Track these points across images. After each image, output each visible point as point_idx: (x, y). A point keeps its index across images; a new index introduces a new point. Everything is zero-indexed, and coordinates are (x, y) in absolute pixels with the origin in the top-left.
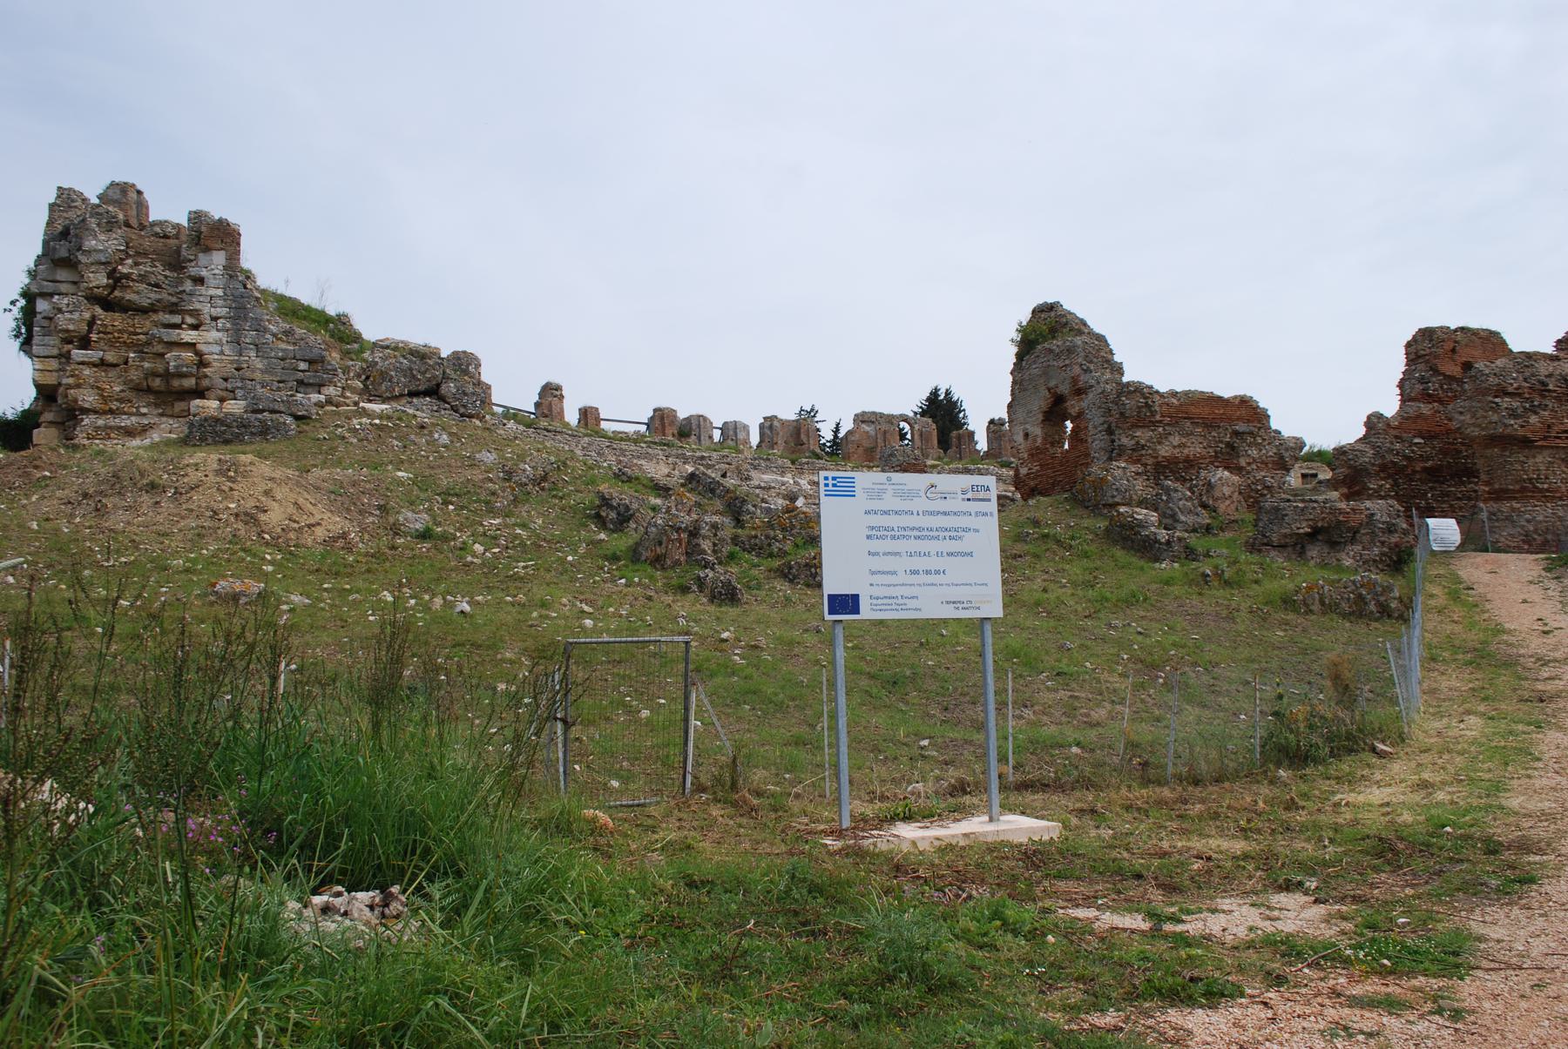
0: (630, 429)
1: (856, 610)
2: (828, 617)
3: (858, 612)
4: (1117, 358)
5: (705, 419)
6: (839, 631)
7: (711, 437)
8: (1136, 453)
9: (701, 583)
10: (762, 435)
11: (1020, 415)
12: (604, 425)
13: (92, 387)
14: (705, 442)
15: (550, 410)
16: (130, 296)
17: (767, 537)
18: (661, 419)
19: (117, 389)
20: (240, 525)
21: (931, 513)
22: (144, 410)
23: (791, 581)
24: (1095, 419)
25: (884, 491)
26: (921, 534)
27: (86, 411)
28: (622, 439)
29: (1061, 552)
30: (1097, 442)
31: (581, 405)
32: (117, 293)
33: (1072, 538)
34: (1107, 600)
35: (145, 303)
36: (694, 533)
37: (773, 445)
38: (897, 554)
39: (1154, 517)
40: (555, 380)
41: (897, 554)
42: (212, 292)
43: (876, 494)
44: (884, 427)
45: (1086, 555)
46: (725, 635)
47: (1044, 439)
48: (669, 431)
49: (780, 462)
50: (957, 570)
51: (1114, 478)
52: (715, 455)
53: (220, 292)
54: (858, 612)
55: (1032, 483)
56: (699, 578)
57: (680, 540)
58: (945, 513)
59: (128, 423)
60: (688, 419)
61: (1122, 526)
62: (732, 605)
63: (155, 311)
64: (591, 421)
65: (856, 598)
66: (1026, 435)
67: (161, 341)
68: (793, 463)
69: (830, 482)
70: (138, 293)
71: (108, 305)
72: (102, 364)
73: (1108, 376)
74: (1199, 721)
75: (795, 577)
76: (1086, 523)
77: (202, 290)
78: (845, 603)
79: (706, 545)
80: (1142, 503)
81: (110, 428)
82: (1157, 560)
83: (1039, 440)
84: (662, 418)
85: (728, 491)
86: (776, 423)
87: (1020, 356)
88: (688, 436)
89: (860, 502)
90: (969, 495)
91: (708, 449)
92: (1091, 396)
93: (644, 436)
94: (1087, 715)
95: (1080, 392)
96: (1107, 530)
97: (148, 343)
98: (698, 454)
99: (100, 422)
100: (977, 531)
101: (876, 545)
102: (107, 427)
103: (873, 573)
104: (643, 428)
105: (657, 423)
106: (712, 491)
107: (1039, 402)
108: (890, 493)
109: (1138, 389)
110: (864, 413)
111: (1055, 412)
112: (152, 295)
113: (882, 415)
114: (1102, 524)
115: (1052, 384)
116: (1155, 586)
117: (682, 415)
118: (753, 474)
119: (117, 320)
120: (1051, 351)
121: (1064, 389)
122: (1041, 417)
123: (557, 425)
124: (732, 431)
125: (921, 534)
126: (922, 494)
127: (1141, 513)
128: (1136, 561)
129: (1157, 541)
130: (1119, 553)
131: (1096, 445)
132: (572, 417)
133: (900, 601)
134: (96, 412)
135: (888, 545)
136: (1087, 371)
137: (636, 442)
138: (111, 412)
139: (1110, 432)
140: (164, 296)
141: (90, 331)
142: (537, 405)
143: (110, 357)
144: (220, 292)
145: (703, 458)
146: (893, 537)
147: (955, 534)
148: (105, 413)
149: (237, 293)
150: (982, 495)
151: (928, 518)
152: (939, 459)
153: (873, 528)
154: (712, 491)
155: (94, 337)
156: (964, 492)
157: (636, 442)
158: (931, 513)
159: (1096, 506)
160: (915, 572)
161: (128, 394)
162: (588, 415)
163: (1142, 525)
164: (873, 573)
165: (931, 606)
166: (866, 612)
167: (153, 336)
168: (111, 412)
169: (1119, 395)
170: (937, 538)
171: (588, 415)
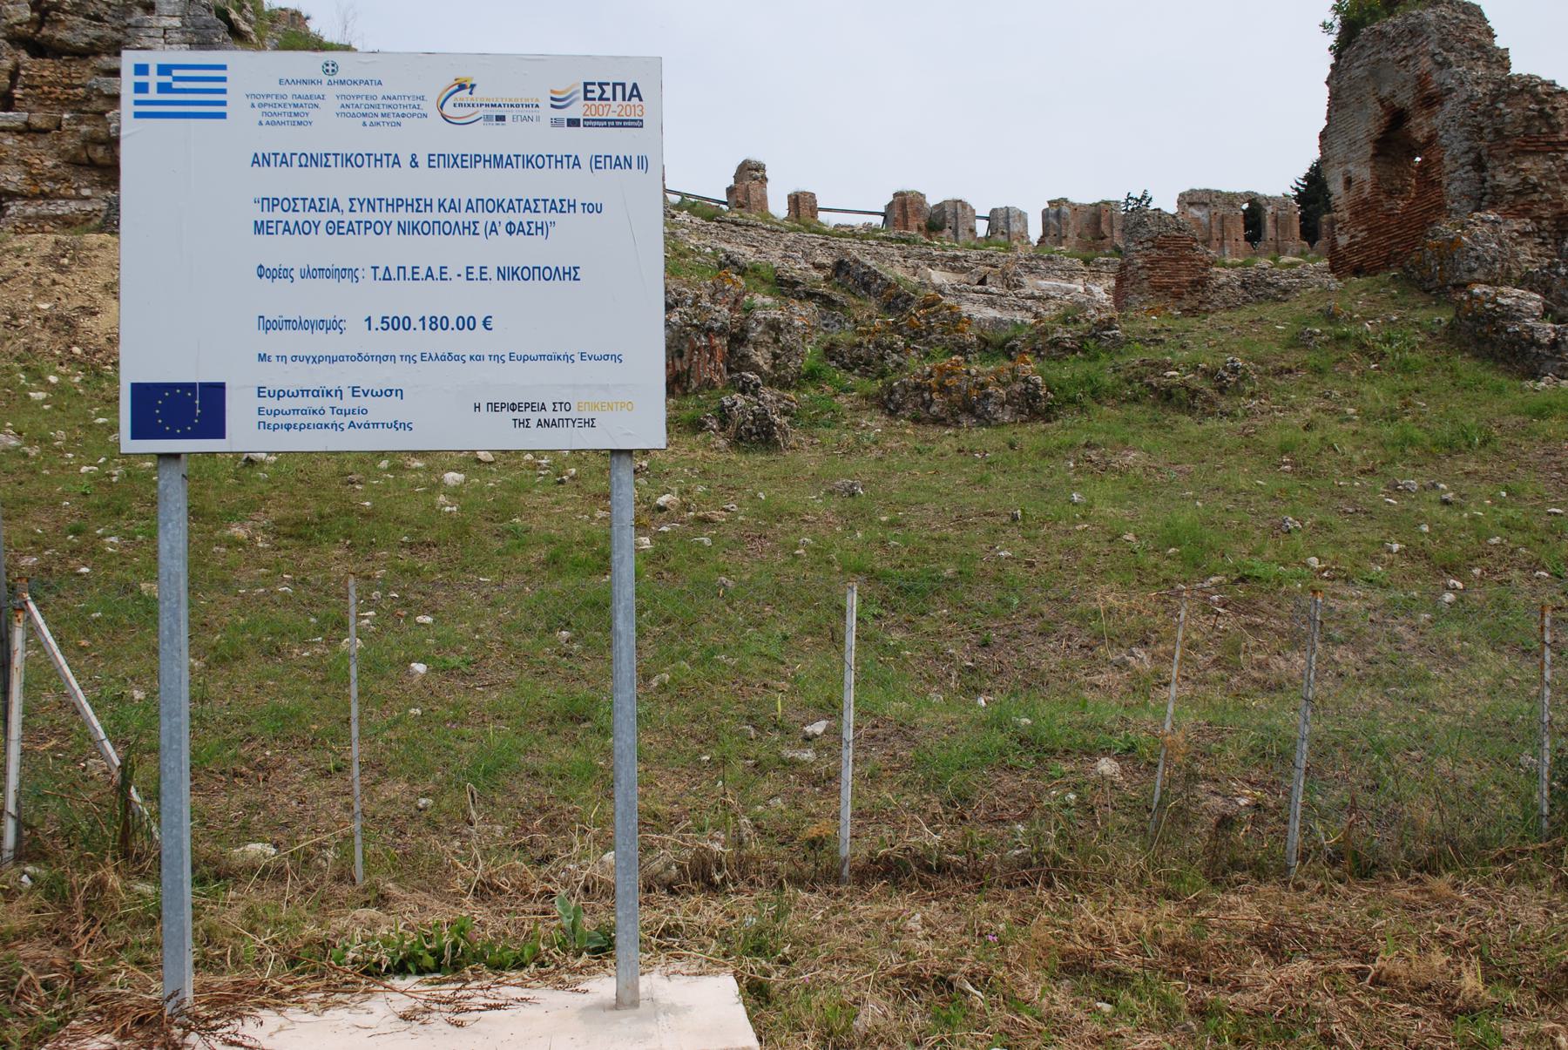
0: (857, 221)
1: (215, 428)
2: (129, 445)
3: (219, 433)
4: (1499, 43)
5: (964, 205)
6: (174, 496)
7: (972, 230)
8: (1521, 201)
9: (724, 416)
10: (1046, 225)
11: (1339, 150)
12: (822, 216)
13: (18, 162)
14: (964, 236)
15: (747, 197)
16: (62, 34)
17: (878, 345)
18: (903, 207)
19: (49, 163)
20: (46, 335)
21: (457, 161)
22: (86, 192)
23: (892, 414)
24: (1455, 144)
25: (314, 101)
26: (417, 218)
27: (12, 196)
28: (843, 235)
29: (1361, 362)
30: (1456, 182)
31: (791, 190)
32: (45, 31)
33: (1389, 340)
34: (1412, 442)
35: (81, 42)
36: (738, 338)
37: (1060, 239)
38: (349, 273)
39: (1534, 301)
40: (755, 156)
41: (349, 273)
42: (166, 22)
43: (273, 110)
44: (1222, 210)
45: (1405, 368)
46: (662, 500)
47: (1376, 186)
48: (913, 223)
49: (1067, 262)
50: (524, 316)
51: (1474, 238)
52: (973, 254)
53: (176, 22)
54: (219, 433)
55: (1356, 260)
56: (722, 409)
57: (712, 349)
58: (497, 161)
59: (66, 210)
60: (941, 206)
61: (1476, 318)
62: (768, 451)
63: (97, 54)
64: (804, 212)
65: (215, 392)
66: (1348, 182)
67: (101, 95)
68: (1086, 263)
69: (153, 79)
70: (71, 29)
71: (39, 49)
72: (28, 130)
73: (1480, 71)
74: (1498, 686)
75: (899, 407)
76: (1420, 315)
77: (153, 20)
78: (188, 408)
79: (761, 358)
80: (1526, 281)
81: (44, 217)
82: (1535, 375)
83: (1368, 188)
84: (903, 205)
85: (889, 286)
86: (1065, 209)
87: (1339, 51)
88: (941, 228)
89: (243, 129)
90: (577, 110)
91: (968, 246)
92: (1449, 106)
93: (876, 230)
94: (1261, 666)
95: (1430, 101)
96: (1452, 327)
97: (87, 99)
98: (950, 253)
99: (30, 210)
100: (593, 208)
101: (279, 249)
102: (39, 217)
103: (268, 325)
104: (879, 220)
105: (897, 212)
106: (866, 286)
107: (1367, 125)
108: (331, 105)
109: (1530, 88)
110: (1193, 192)
111: (1394, 140)
112: (91, 32)
113: (1218, 194)
114: (1445, 317)
115: (1386, 91)
116: (1514, 419)
117: (932, 200)
118: (1025, 279)
119: (47, 69)
120: (1382, 34)
121: (1405, 98)
122: (1369, 149)
123: (752, 217)
124: (1002, 221)
125: (417, 218)
126: (430, 107)
127: (1510, 296)
128: (1492, 377)
129: (1534, 342)
130: (1464, 364)
131: (1455, 188)
132: (778, 207)
133: (349, 402)
134: (25, 197)
135: (322, 249)
136: (1444, 65)
137: (862, 238)
138: (43, 195)
139: (1479, 165)
140: (107, 32)
141: (13, 85)
142: (730, 191)
143: (38, 120)
144: (176, 22)
145: (955, 258)
146: (335, 228)
147: (525, 219)
148: (35, 197)
149: (199, 22)
150: (614, 110)
151: (442, 173)
152: (1302, 254)
153: (273, 203)
154: (866, 286)
155: (18, 93)
156: (558, 102)
157: (862, 238)
158: (457, 161)
159: (1442, 288)
160: (402, 323)
161: (62, 171)
162: (801, 204)
163: (1510, 314)
164: (268, 325)
165: (442, 412)
166: (244, 431)
167: (90, 89)
168: (43, 195)
169: (1495, 99)
170: (470, 229)
171: (801, 204)
